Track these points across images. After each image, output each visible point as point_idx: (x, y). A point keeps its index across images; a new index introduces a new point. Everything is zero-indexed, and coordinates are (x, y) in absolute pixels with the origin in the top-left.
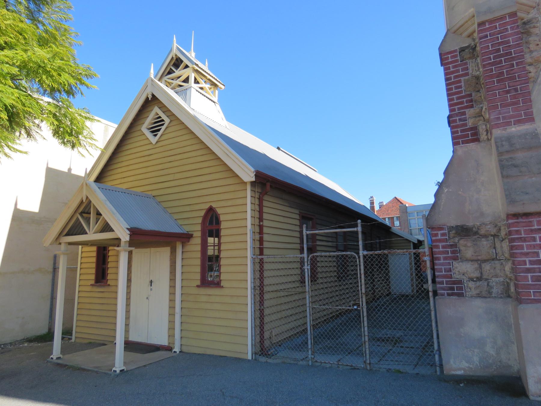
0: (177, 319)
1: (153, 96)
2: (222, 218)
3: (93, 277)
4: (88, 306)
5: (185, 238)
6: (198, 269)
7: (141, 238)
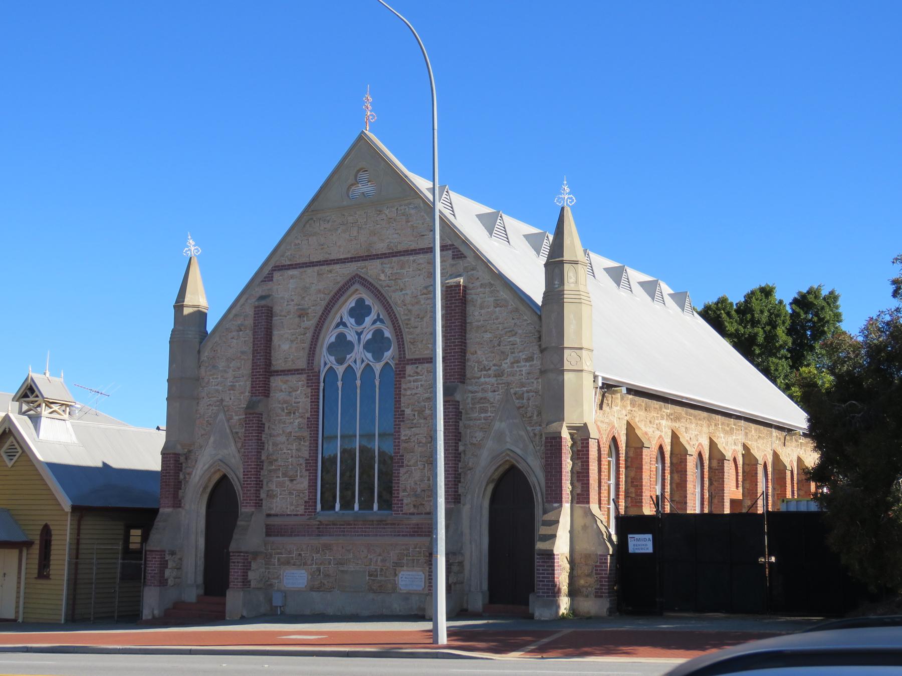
2: (53, 532)
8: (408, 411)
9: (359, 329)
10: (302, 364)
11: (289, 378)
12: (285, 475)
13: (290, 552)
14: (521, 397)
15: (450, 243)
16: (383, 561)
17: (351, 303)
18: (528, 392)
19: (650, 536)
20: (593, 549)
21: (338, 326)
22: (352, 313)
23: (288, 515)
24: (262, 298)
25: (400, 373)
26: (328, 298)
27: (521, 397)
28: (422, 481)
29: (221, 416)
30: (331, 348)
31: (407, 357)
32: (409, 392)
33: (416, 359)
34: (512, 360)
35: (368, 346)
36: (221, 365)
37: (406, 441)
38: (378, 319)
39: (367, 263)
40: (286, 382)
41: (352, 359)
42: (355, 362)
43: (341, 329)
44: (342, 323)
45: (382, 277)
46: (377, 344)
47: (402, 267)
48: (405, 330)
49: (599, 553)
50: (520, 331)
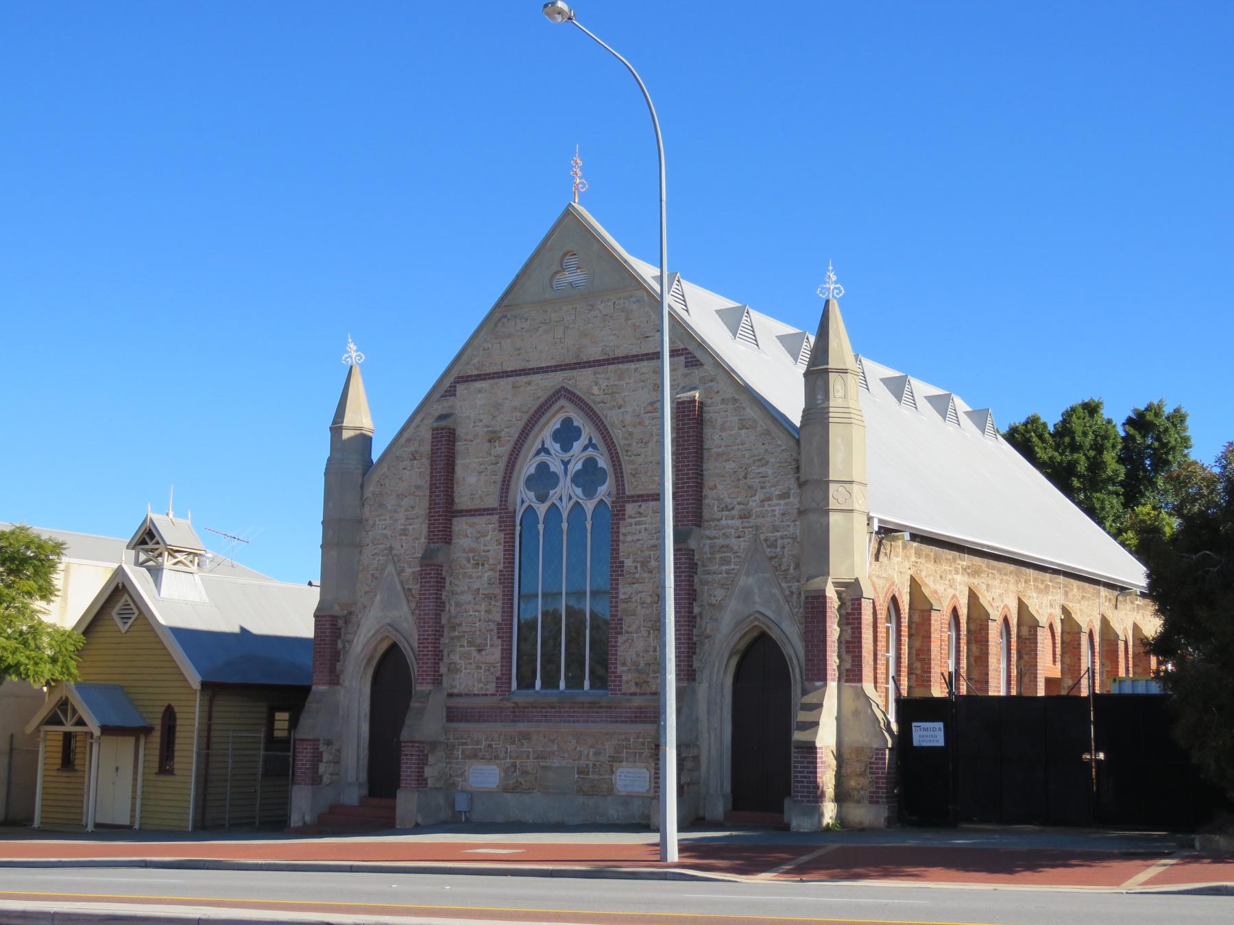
0: (138, 802)
1: (124, 585)
2: (178, 716)
3: (59, 761)
4: (53, 791)
5: (147, 730)
6: (157, 759)
7: (106, 730)
8: (628, 563)
9: (566, 456)
10: (492, 502)
11: (477, 519)
12: (470, 644)
13: (478, 743)
14: (773, 545)
15: (682, 346)
16: (596, 754)
17: (556, 424)
18: (782, 538)
19: (941, 725)
20: (867, 740)
21: (538, 453)
22: (556, 436)
23: (475, 695)
24: (442, 417)
25: (618, 514)
26: (526, 417)
27: (773, 545)
28: (646, 651)
29: (390, 568)
30: (530, 482)
31: (628, 493)
32: (629, 538)
33: (639, 496)
34: (762, 497)
35: (576, 479)
36: (390, 502)
37: (627, 601)
38: (590, 444)
39: (575, 373)
40: (472, 525)
41: (557, 496)
42: (561, 499)
43: (543, 457)
44: (544, 450)
45: (595, 390)
46: (588, 477)
47: (621, 378)
48: (624, 459)
49: (875, 746)
50: (772, 460)
